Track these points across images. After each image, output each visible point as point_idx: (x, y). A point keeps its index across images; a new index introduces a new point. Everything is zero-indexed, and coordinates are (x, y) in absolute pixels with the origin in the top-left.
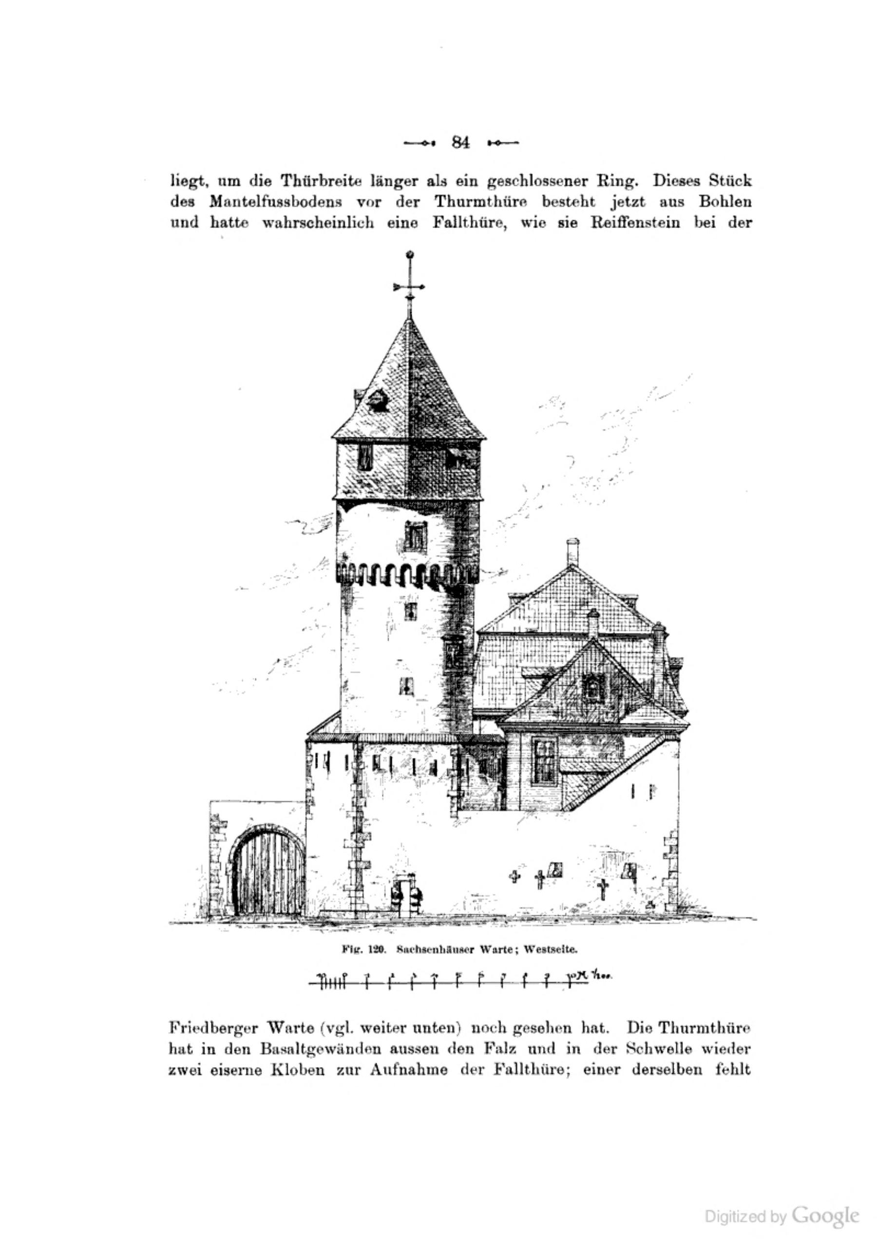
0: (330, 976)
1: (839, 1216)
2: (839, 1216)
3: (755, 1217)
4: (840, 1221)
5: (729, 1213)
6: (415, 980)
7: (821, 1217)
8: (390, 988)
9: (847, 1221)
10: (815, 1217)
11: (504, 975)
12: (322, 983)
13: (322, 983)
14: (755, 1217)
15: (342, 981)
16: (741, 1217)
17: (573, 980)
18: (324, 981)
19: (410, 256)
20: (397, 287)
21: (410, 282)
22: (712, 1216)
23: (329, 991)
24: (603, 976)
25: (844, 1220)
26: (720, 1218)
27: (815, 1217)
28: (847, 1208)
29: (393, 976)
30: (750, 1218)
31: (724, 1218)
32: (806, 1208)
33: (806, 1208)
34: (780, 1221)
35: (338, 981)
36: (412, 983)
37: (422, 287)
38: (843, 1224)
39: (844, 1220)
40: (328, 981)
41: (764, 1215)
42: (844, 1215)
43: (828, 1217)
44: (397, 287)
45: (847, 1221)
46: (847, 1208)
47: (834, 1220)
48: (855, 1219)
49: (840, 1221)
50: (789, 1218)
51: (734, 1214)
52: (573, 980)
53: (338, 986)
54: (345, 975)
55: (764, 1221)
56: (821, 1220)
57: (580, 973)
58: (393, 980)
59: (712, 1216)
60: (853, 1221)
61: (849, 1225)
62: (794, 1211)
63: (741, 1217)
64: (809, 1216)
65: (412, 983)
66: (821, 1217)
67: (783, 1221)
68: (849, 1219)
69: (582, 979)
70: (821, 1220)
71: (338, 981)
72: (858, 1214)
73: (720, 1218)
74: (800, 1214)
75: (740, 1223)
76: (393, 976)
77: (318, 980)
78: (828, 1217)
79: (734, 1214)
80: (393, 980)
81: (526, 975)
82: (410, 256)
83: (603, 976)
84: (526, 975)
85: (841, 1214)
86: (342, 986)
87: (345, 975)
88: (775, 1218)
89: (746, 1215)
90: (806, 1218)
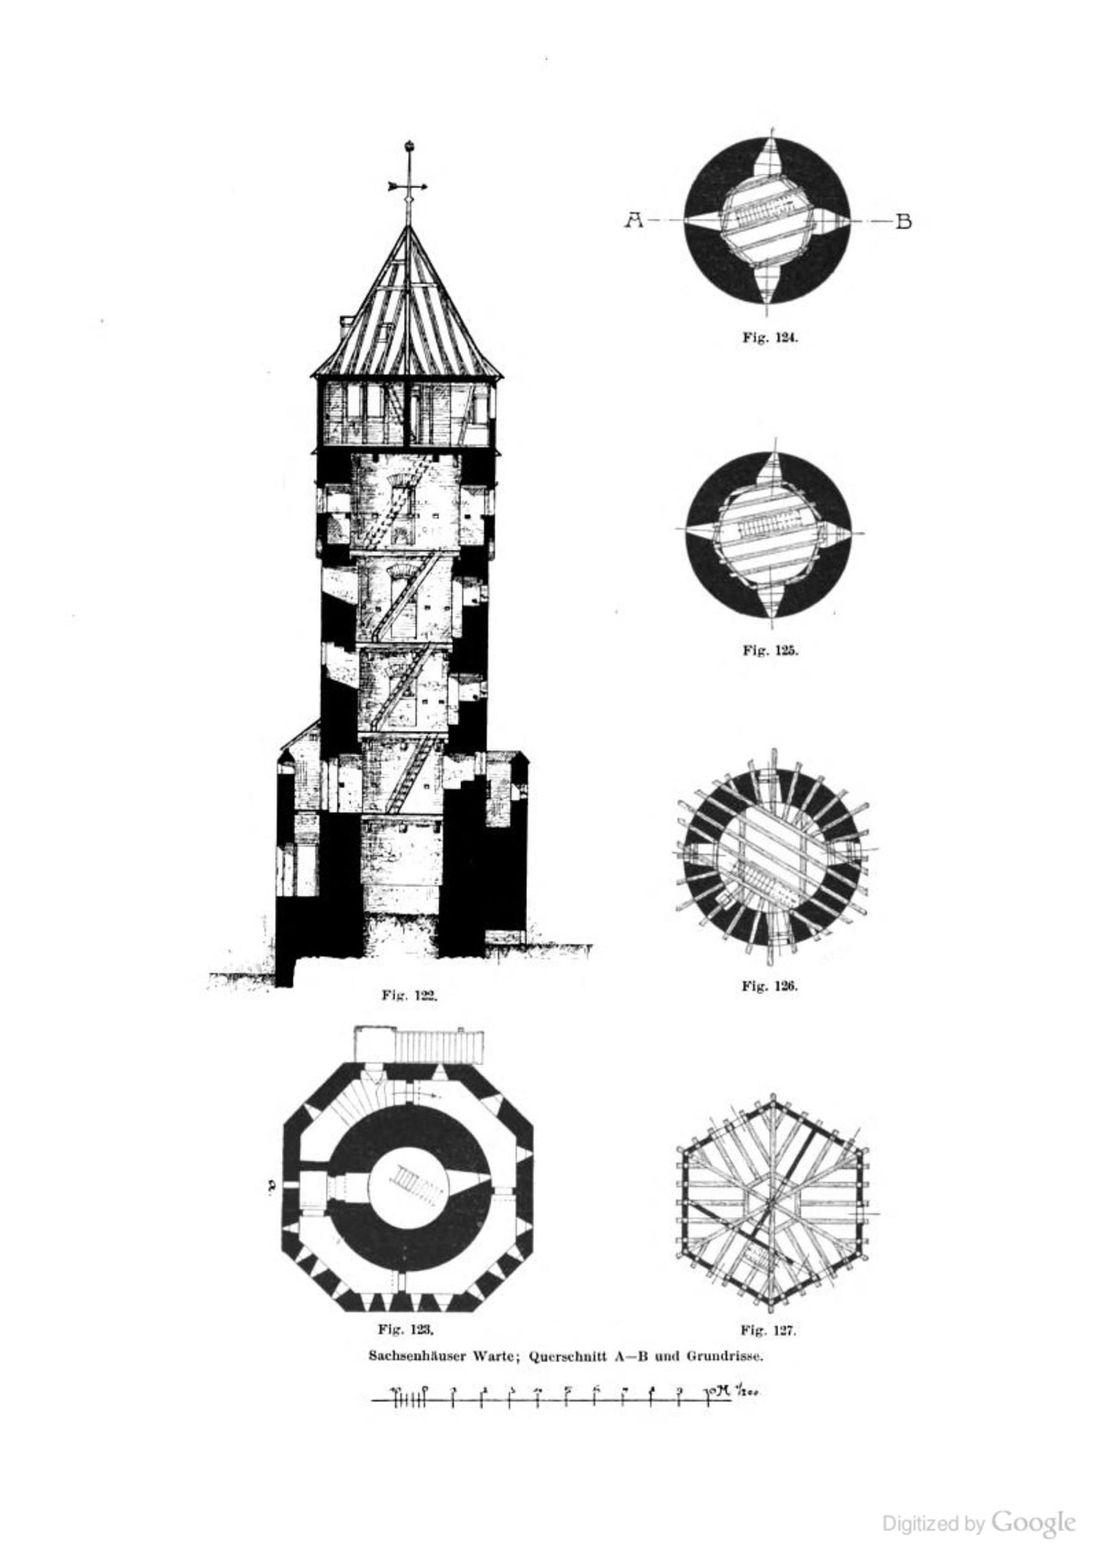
0: (406, 1391)
1: (1050, 1523)
2: (1050, 1523)
3: (944, 1525)
4: (1052, 1529)
5: (913, 1519)
6: (513, 1396)
7: (1028, 1524)
8: (482, 1406)
9: (1061, 1529)
10: (1021, 1524)
11: (626, 1389)
12: (396, 1400)
13: (396, 1400)
14: (944, 1525)
15: (422, 1397)
16: (928, 1524)
17: (712, 1397)
18: (398, 1397)
19: (409, 147)
20: (393, 187)
21: (409, 180)
22: (893, 1523)
23: (405, 1410)
24: (750, 1393)
25: (1056, 1528)
26: (901, 1525)
27: (1021, 1524)
28: (1061, 1513)
29: (485, 1391)
30: (939, 1524)
31: (907, 1525)
32: (1009, 1513)
33: (1009, 1513)
34: (977, 1529)
35: (416, 1397)
36: (509, 1400)
37: (424, 187)
38: (1055, 1533)
39: (1056, 1528)
40: (404, 1397)
41: (957, 1522)
42: (1057, 1521)
43: (1036, 1524)
44: (393, 187)
45: (1061, 1529)
46: (1061, 1513)
47: (1045, 1529)
48: (1071, 1526)
49: (1052, 1529)
50: (988, 1524)
51: (919, 1520)
52: (713, 1397)
53: (416, 1403)
54: (425, 1389)
55: (957, 1528)
56: (1028, 1528)
57: (721, 1387)
58: (485, 1396)
59: (893, 1523)
60: (1068, 1529)
61: (1062, 1535)
62: (995, 1516)
63: (928, 1524)
64: (1012, 1522)
65: (509, 1400)
66: (1028, 1524)
67: (981, 1529)
68: (1063, 1527)
69: (724, 1396)
70: (1028, 1528)
71: (416, 1397)
72: (1074, 1520)
73: (901, 1525)
74: (1002, 1521)
75: (927, 1532)
76: (485, 1391)
77: (392, 1396)
78: (1036, 1524)
79: (919, 1520)
80: (485, 1396)
81: (653, 1389)
82: (409, 147)
83: (750, 1393)
84: (653, 1389)
85: (1053, 1520)
86: (422, 1403)
87: (425, 1389)
88: (970, 1525)
89: (933, 1521)
90: (1010, 1525)
